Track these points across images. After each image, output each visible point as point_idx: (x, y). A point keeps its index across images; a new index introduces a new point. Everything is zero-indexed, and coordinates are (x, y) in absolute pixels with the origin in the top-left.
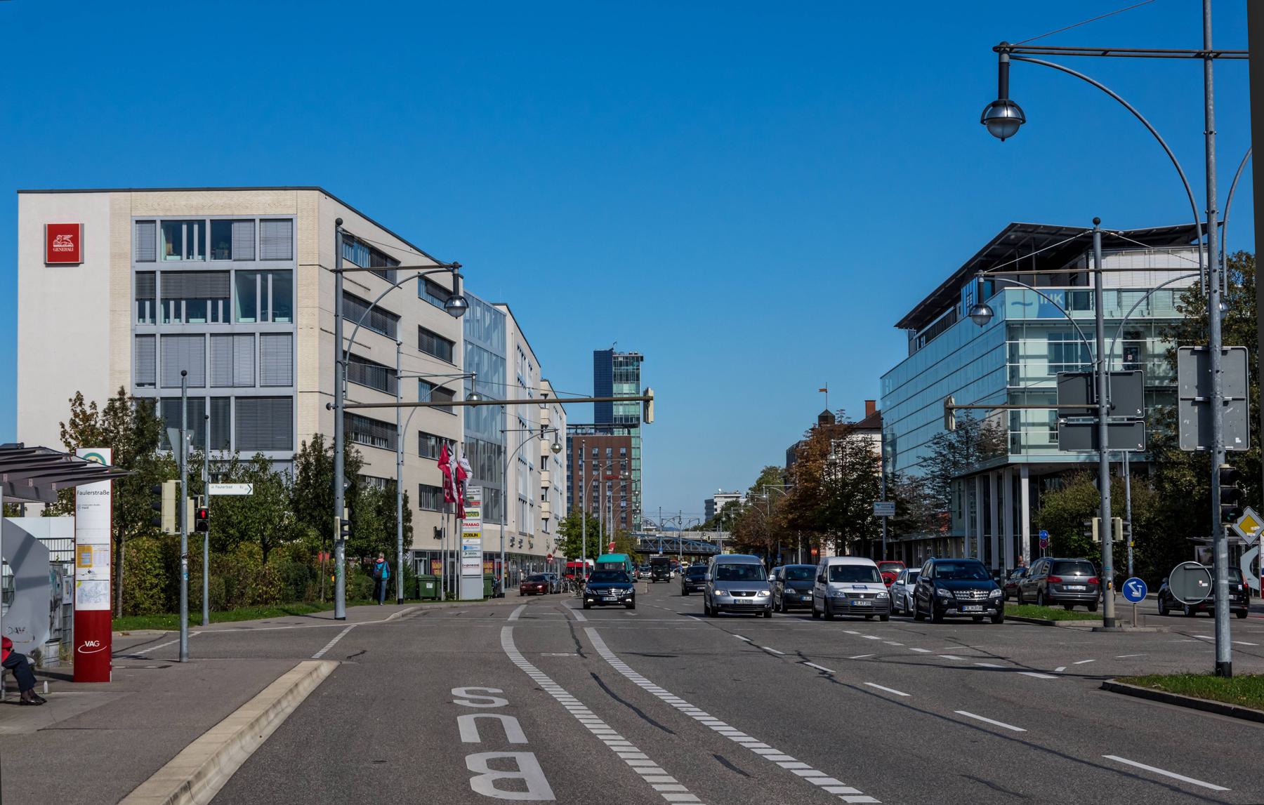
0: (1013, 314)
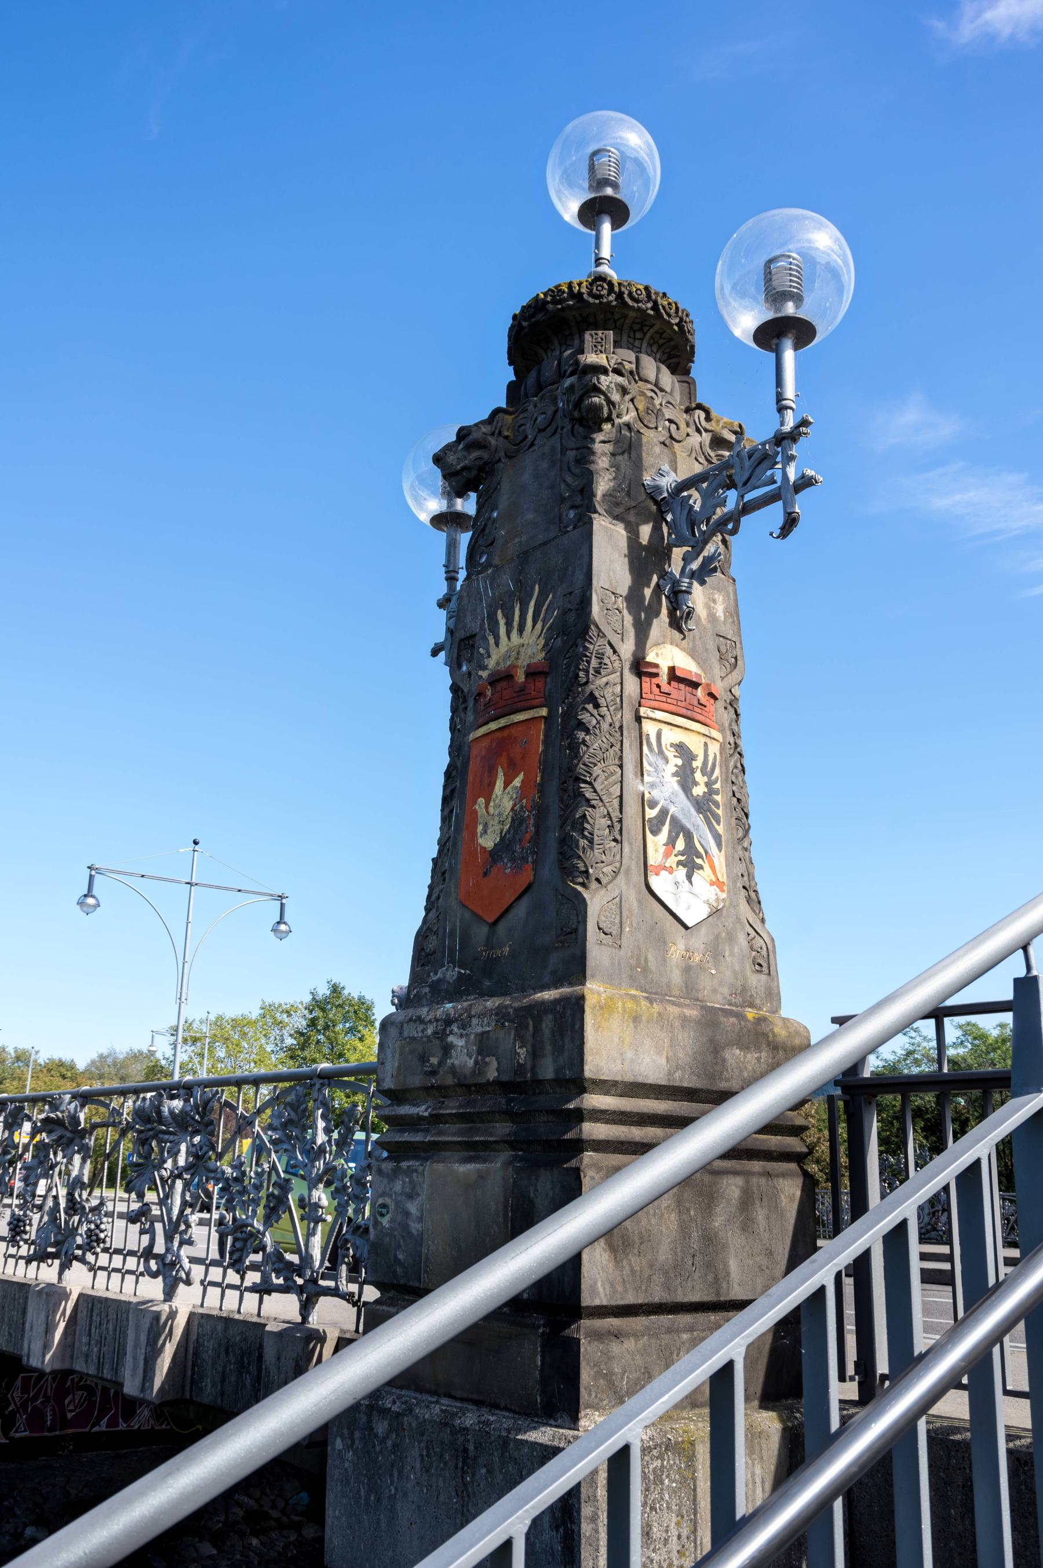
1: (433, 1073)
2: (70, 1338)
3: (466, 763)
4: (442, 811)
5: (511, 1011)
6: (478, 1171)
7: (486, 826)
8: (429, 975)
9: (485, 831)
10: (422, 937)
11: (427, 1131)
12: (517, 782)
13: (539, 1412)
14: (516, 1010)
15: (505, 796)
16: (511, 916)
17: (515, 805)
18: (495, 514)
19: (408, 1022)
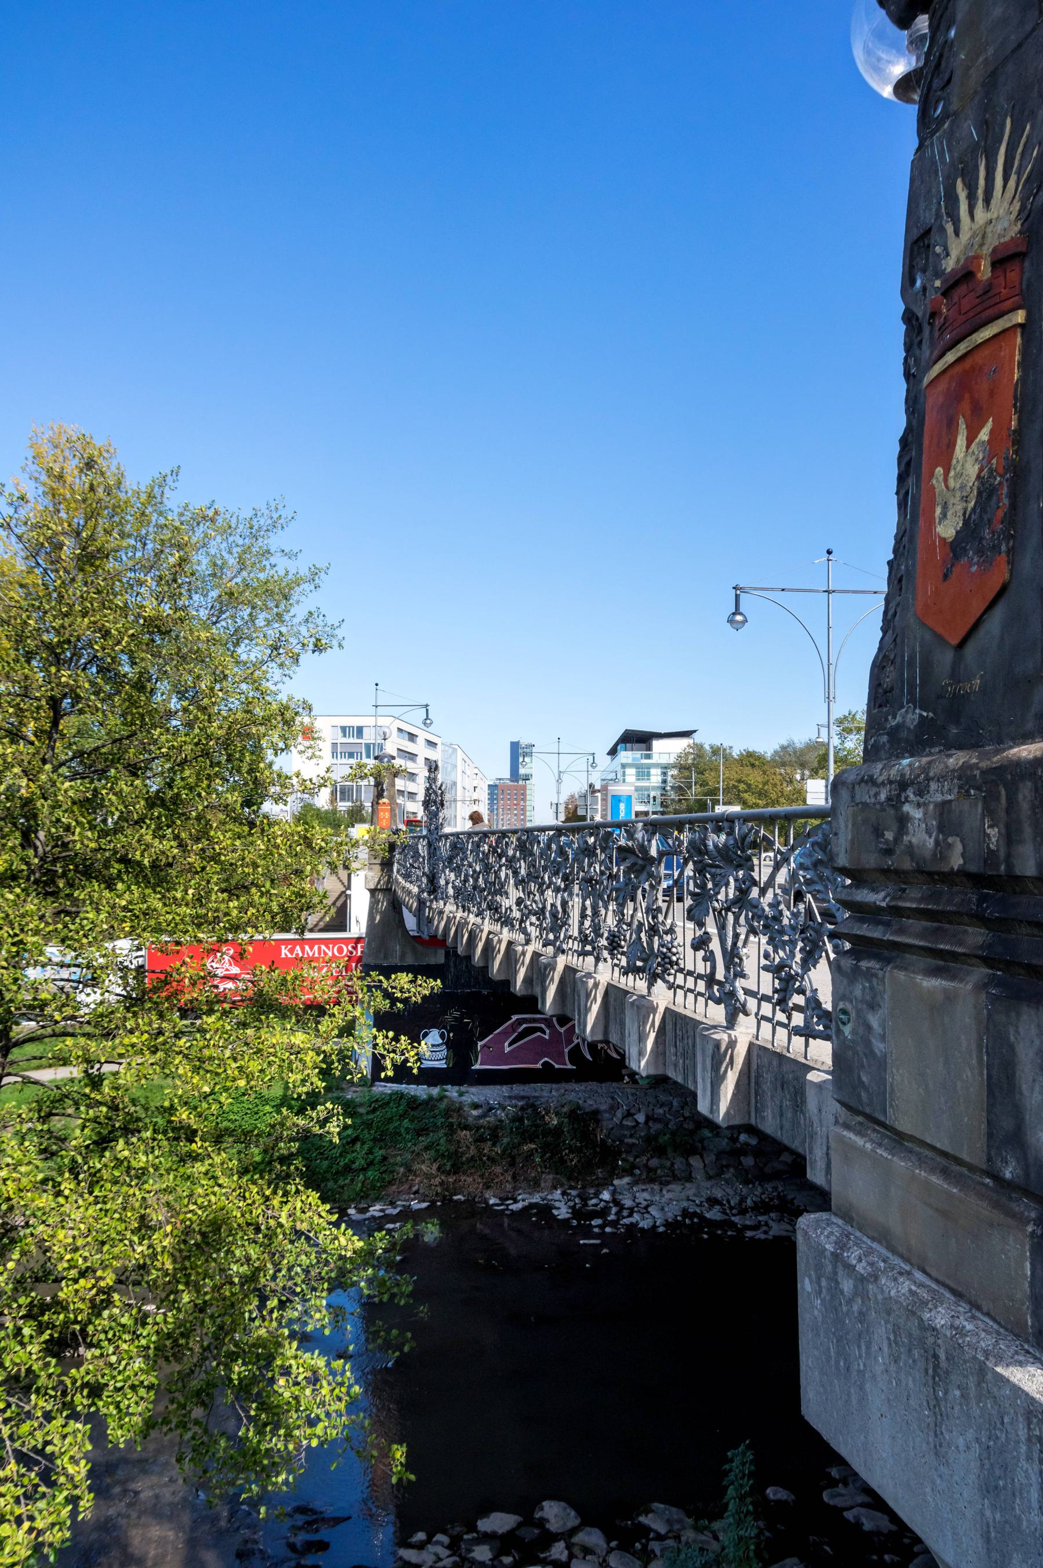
0: (624, 761)
1: (889, 852)
2: (661, 1048)
3: (922, 423)
4: (897, 493)
5: (977, 772)
6: (945, 990)
7: (945, 507)
8: (887, 720)
9: (944, 515)
10: (879, 667)
11: (888, 924)
12: (984, 435)
13: (1030, 1339)
14: (983, 772)
15: (969, 458)
16: (982, 632)
17: (981, 470)
18: (953, 33)
19: (859, 784)
